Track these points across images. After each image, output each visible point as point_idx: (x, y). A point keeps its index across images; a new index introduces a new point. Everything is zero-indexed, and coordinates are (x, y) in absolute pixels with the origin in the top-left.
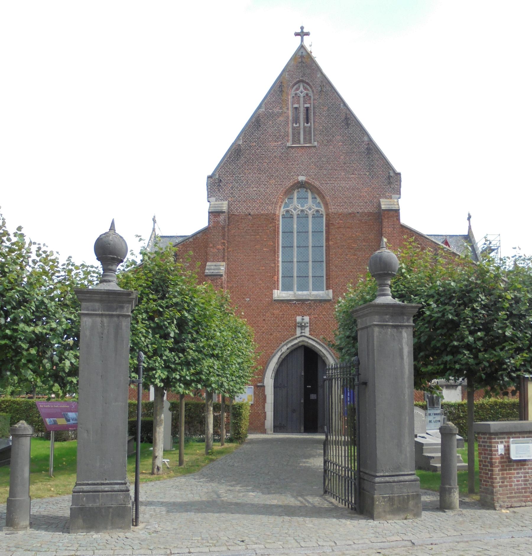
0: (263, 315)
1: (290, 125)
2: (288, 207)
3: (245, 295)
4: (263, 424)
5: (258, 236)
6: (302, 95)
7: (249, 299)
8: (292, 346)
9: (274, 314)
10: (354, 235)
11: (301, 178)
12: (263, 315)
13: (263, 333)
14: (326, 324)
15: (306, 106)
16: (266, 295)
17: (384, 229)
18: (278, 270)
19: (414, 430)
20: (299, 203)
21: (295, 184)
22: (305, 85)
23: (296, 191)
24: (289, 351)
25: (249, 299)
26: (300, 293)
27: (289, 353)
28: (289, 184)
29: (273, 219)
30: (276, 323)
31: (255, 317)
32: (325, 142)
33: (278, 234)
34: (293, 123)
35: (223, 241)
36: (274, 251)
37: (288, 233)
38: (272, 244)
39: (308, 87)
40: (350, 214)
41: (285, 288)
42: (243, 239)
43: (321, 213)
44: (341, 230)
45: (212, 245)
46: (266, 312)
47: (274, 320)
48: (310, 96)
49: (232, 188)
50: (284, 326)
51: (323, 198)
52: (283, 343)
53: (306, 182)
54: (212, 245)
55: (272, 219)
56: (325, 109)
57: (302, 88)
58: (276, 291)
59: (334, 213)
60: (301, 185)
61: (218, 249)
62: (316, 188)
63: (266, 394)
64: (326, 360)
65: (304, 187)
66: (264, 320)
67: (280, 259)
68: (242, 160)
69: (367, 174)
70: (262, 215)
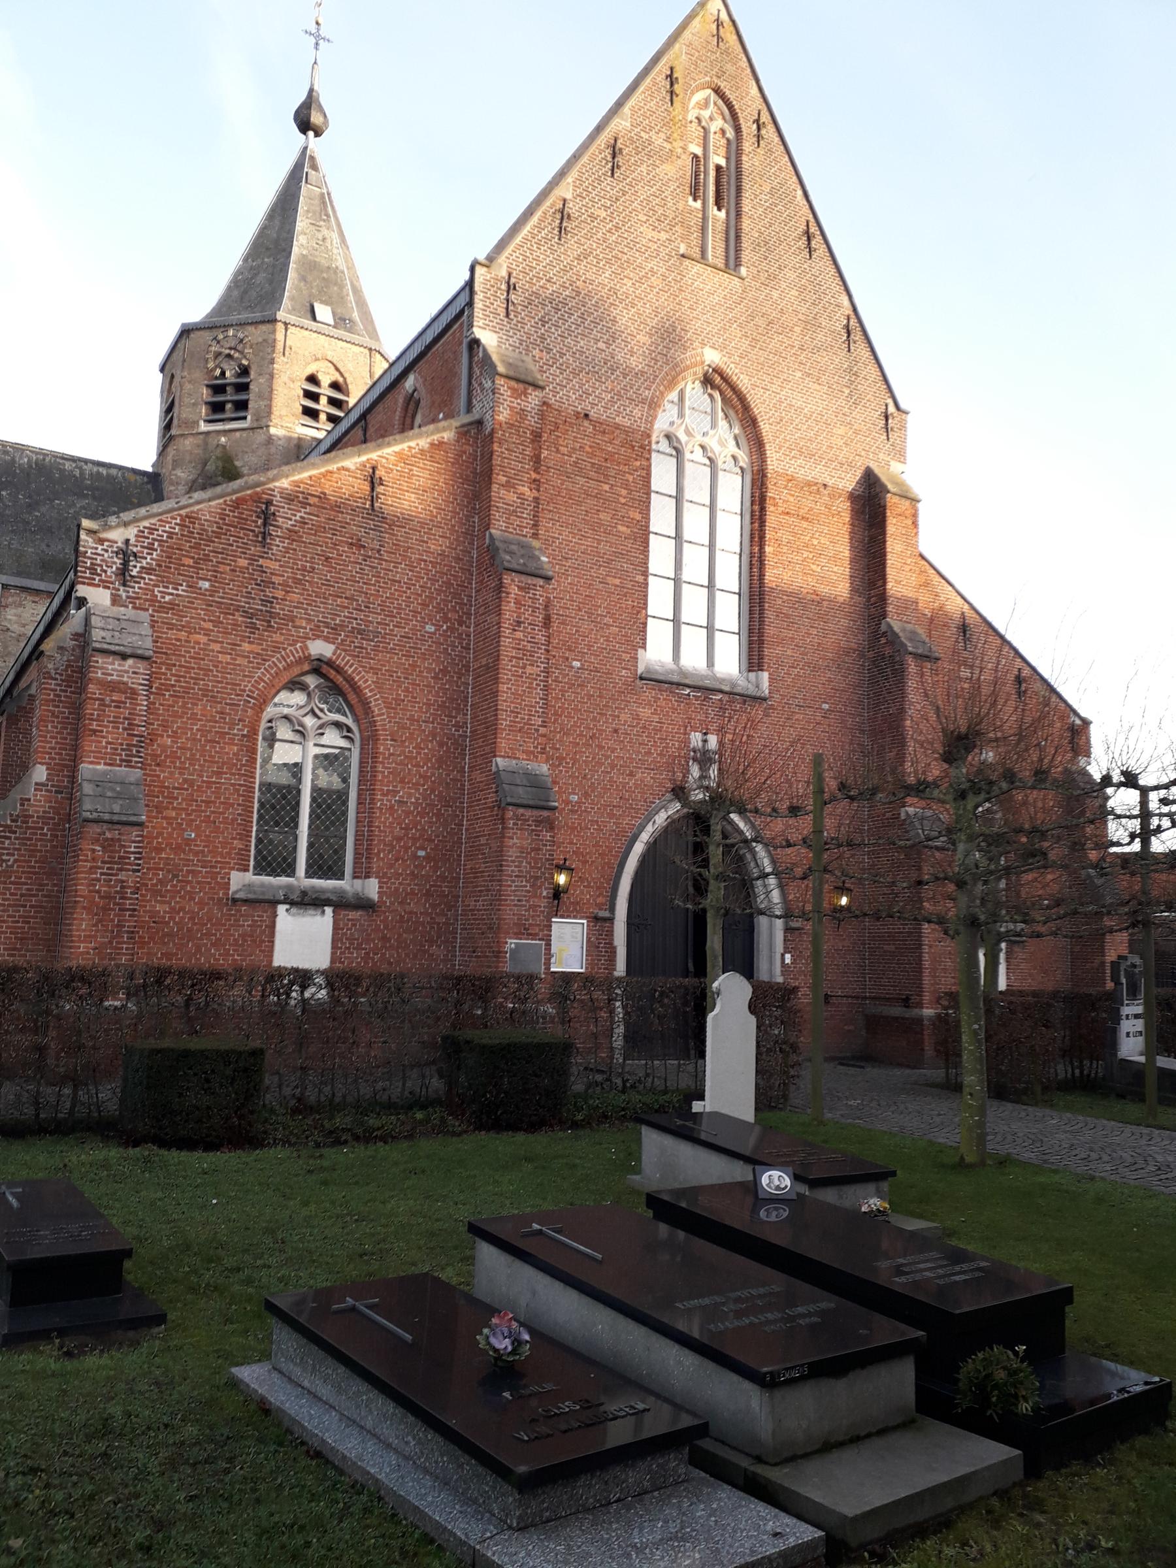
5: (606, 487)
35: (534, 476)
70: (617, 426)
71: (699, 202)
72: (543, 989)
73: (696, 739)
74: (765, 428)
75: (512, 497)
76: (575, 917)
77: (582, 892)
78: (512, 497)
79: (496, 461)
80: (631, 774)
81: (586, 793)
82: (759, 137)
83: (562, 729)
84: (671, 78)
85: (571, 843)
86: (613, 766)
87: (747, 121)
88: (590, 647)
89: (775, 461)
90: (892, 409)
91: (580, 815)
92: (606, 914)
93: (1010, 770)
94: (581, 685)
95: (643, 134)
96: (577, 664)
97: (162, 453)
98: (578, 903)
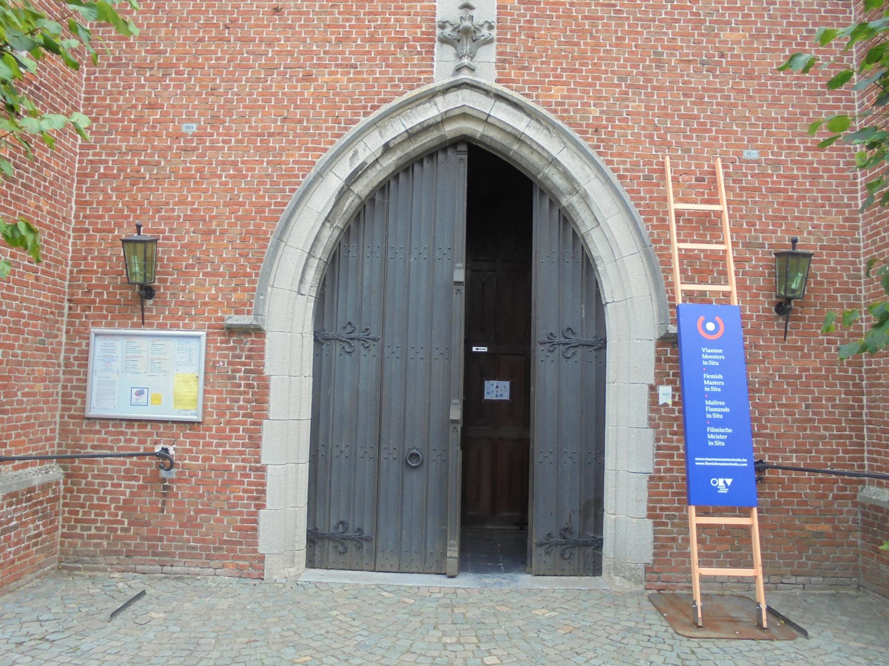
76: (186, 327)
77: (201, 284)
80: (308, 77)
81: (215, 117)
83: (171, 20)
85: (183, 202)
86: (270, 69)
91: (203, 155)
93: (777, 311)
97: (105, 421)
98: (193, 304)
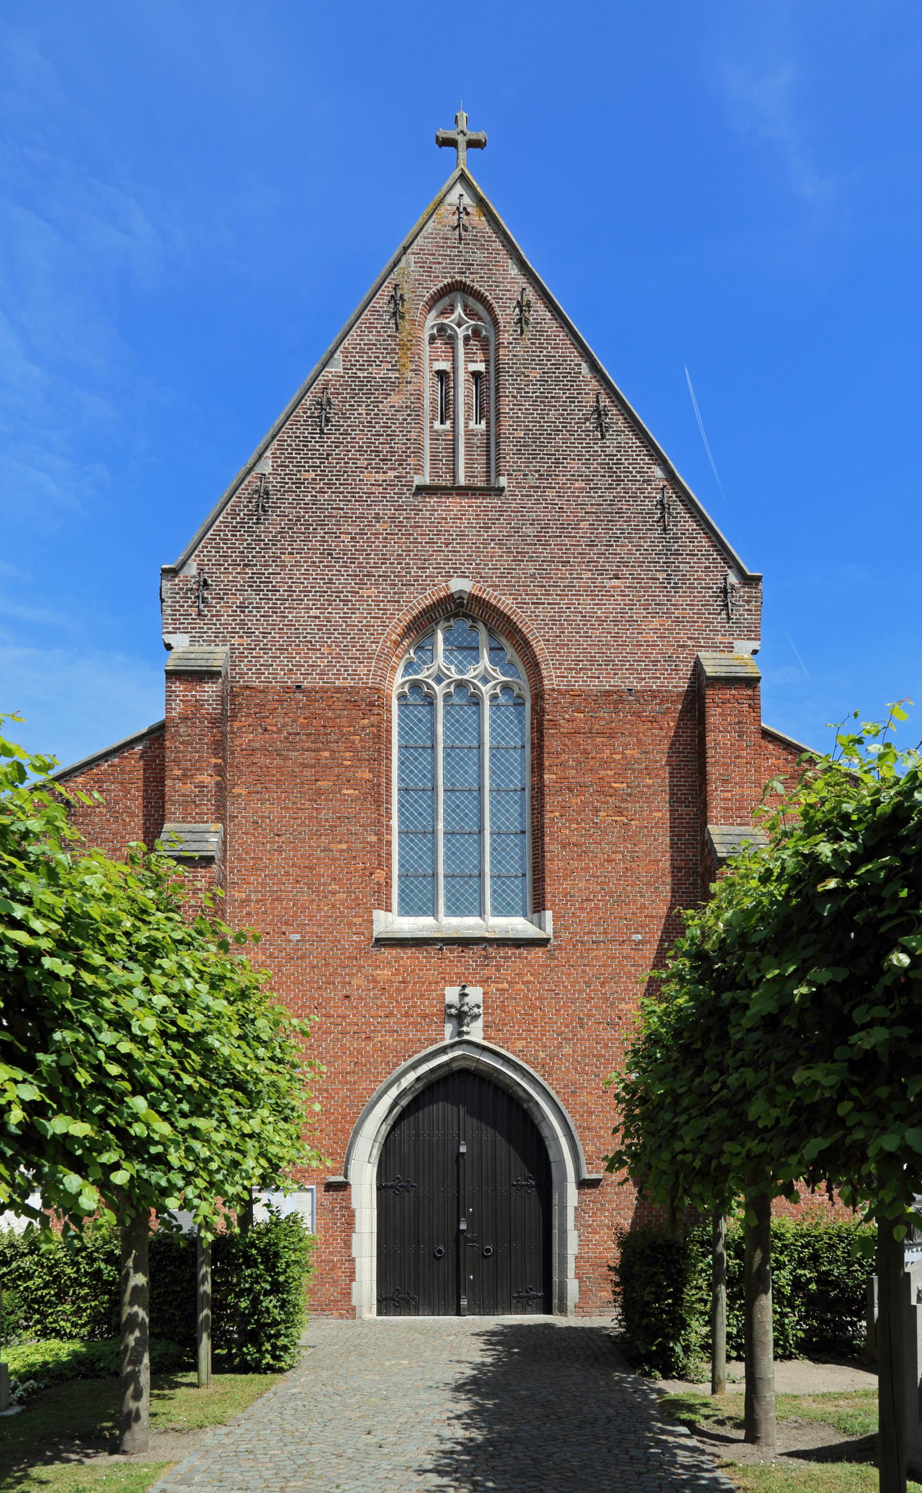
0: (344, 984)
1: (427, 425)
2: (417, 673)
3: (287, 924)
4: (347, 1294)
5: (327, 754)
6: (461, 332)
7: (298, 937)
8: (432, 1071)
9: (375, 981)
10: (618, 757)
11: (458, 585)
12: (344, 984)
13: (344, 1033)
14: (533, 1007)
15: (473, 367)
16: (350, 924)
17: (710, 738)
18: (389, 854)
19: (872, 1437)
20: (451, 663)
21: (441, 601)
22: (471, 301)
23: (443, 625)
24: (420, 1085)
25: (298, 937)
26: (455, 921)
27: (423, 1092)
28: (421, 600)
29: (371, 704)
30: (383, 1005)
31: (320, 988)
32: (532, 480)
33: (389, 749)
34: (433, 419)
36: (377, 796)
37: (419, 748)
38: (368, 775)
39: (479, 308)
40: (607, 693)
41: (407, 910)
42: (278, 761)
43: (516, 691)
44: (580, 739)
45: (179, 773)
46: (352, 975)
47: (376, 997)
48: (486, 339)
49: (242, 607)
50: (407, 1015)
51: (523, 645)
52: (404, 1065)
53: (474, 598)
54: (179, 773)
55: (372, 702)
56: (535, 375)
57: (459, 310)
58: (382, 913)
59: (559, 691)
60: (455, 608)
61: (201, 786)
62: (502, 614)
63: (353, 1206)
64: (534, 1109)
65: (466, 616)
66: (347, 997)
67: (395, 822)
68: (273, 524)
69: (661, 576)
70: (338, 690)
71: (448, 425)
72: (193, 1270)
73: (451, 994)
74: (539, 647)
75: (188, 788)
78: (188, 788)
79: (170, 756)
82: (521, 321)
84: (396, 299)
87: (504, 308)
88: (311, 917)
89: (552, 679)
90: (733, 579)
92: (341, 1179)
94: (302, 957)
95: (359, 374)
96: (296, 937)
